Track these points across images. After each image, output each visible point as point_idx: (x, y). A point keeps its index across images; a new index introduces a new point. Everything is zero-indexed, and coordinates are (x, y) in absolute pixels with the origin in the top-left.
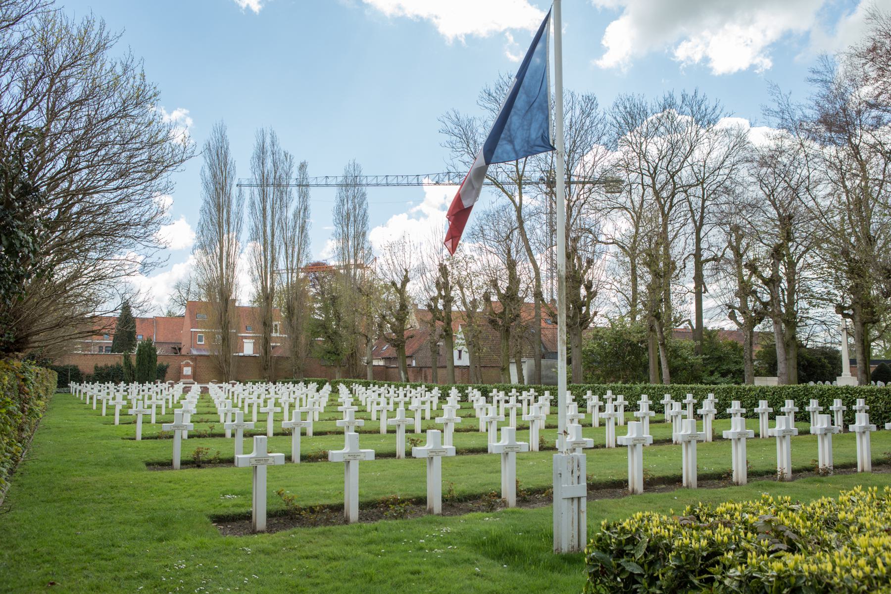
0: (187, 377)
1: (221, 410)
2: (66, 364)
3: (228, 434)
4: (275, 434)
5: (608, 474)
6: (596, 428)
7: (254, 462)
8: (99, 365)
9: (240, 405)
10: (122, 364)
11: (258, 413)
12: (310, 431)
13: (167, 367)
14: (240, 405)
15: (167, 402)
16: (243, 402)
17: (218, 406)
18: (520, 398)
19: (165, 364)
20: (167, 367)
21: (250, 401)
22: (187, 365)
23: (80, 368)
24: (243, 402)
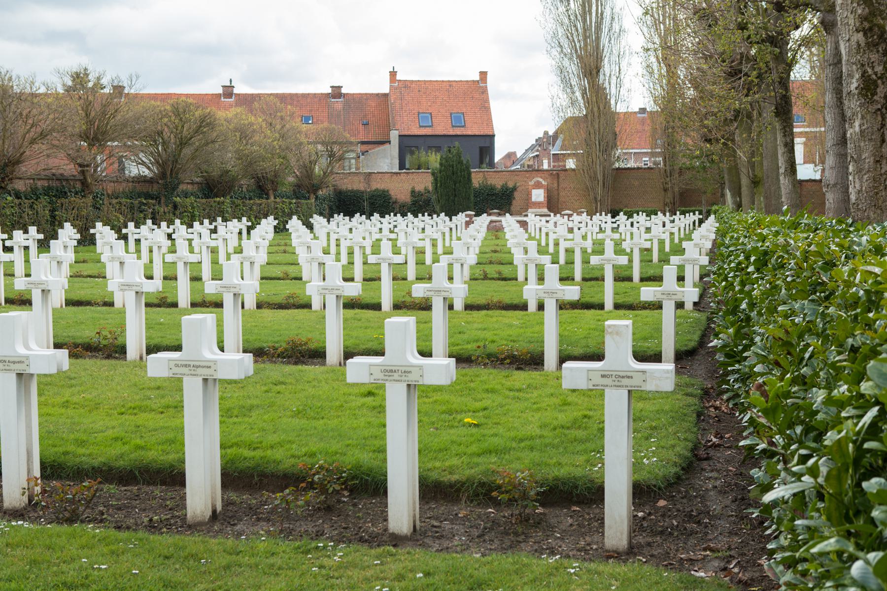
0: (538, 205)
1: (518, 257)
2: (374, 188)
3: (532, 306)
4: (259, 306)
5: (106, 439)
6: (458, 313)
7: (381, 376)
8: (417, 189)
9: (551, 249)
10: (430, 189)
11: (365, 263)
12: (458, 305)
13: (515, 189)
14: (551, 249)
15: (434, 245)
16: (338, 245)
17: (298, 251)
18: (8, 243)
19: (511, 185)
20: (515, 189)
21: (568, 244)
22: (538, 186)
23: (392, 193)
24: (338, 245)
